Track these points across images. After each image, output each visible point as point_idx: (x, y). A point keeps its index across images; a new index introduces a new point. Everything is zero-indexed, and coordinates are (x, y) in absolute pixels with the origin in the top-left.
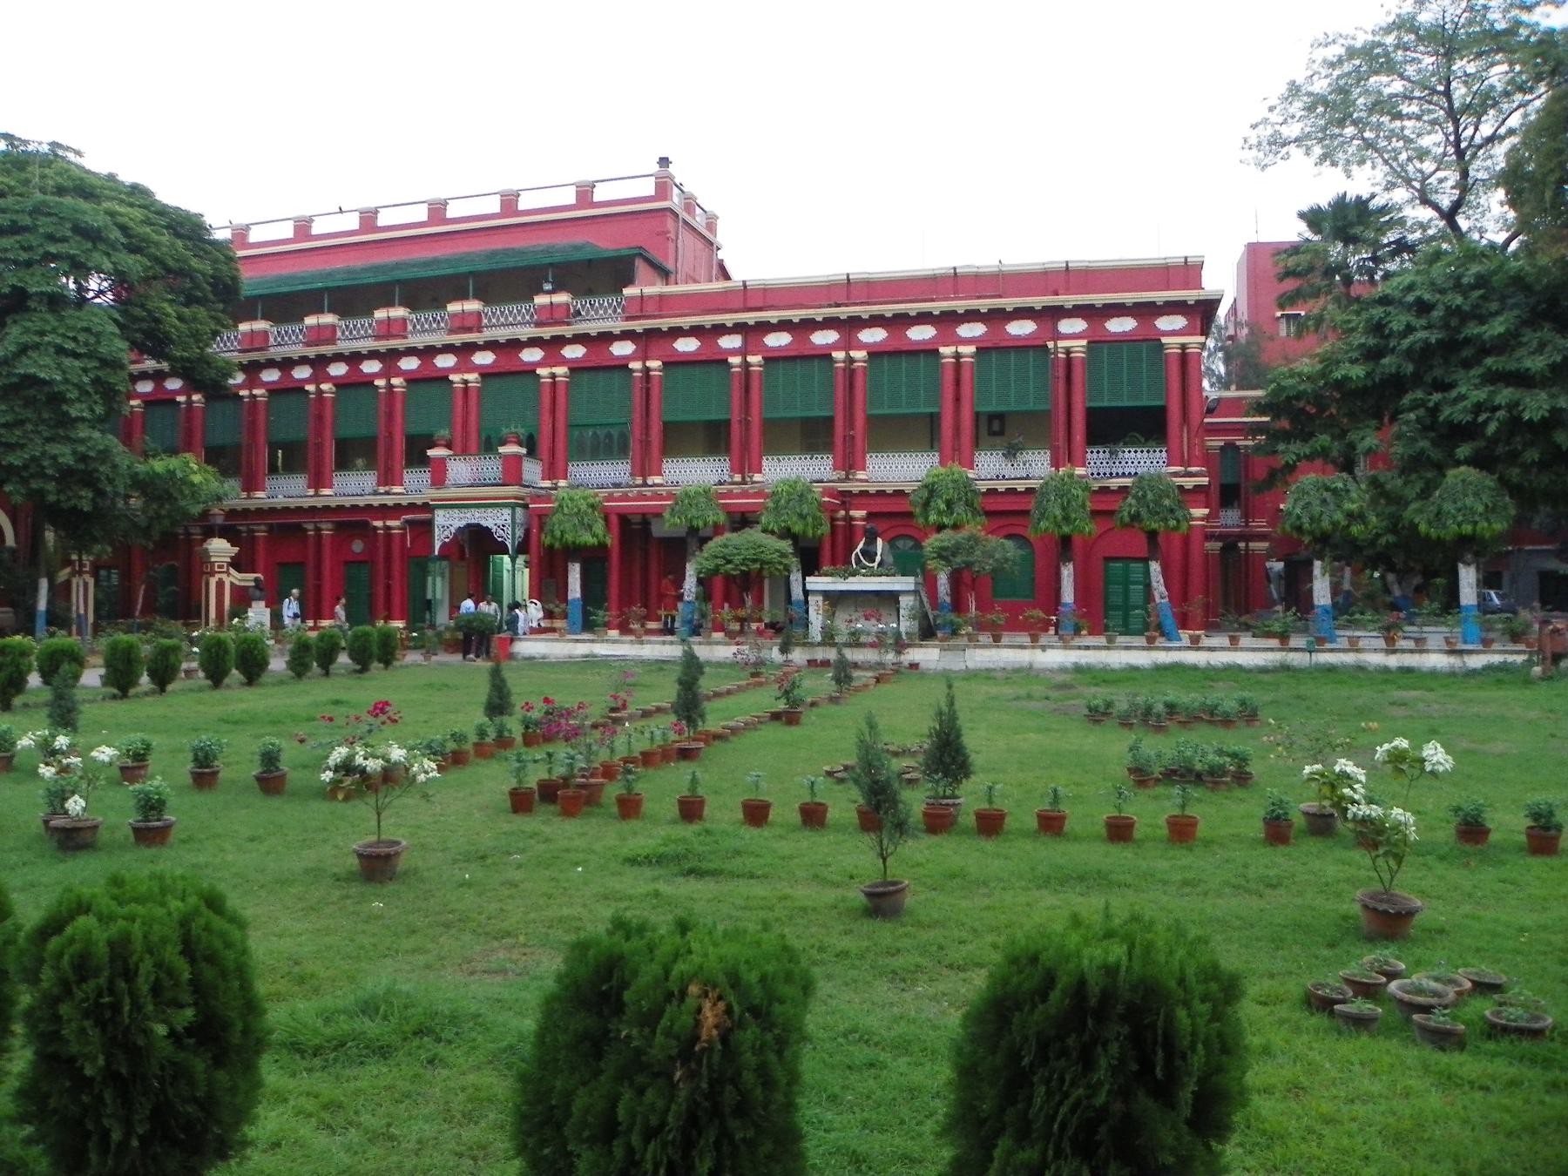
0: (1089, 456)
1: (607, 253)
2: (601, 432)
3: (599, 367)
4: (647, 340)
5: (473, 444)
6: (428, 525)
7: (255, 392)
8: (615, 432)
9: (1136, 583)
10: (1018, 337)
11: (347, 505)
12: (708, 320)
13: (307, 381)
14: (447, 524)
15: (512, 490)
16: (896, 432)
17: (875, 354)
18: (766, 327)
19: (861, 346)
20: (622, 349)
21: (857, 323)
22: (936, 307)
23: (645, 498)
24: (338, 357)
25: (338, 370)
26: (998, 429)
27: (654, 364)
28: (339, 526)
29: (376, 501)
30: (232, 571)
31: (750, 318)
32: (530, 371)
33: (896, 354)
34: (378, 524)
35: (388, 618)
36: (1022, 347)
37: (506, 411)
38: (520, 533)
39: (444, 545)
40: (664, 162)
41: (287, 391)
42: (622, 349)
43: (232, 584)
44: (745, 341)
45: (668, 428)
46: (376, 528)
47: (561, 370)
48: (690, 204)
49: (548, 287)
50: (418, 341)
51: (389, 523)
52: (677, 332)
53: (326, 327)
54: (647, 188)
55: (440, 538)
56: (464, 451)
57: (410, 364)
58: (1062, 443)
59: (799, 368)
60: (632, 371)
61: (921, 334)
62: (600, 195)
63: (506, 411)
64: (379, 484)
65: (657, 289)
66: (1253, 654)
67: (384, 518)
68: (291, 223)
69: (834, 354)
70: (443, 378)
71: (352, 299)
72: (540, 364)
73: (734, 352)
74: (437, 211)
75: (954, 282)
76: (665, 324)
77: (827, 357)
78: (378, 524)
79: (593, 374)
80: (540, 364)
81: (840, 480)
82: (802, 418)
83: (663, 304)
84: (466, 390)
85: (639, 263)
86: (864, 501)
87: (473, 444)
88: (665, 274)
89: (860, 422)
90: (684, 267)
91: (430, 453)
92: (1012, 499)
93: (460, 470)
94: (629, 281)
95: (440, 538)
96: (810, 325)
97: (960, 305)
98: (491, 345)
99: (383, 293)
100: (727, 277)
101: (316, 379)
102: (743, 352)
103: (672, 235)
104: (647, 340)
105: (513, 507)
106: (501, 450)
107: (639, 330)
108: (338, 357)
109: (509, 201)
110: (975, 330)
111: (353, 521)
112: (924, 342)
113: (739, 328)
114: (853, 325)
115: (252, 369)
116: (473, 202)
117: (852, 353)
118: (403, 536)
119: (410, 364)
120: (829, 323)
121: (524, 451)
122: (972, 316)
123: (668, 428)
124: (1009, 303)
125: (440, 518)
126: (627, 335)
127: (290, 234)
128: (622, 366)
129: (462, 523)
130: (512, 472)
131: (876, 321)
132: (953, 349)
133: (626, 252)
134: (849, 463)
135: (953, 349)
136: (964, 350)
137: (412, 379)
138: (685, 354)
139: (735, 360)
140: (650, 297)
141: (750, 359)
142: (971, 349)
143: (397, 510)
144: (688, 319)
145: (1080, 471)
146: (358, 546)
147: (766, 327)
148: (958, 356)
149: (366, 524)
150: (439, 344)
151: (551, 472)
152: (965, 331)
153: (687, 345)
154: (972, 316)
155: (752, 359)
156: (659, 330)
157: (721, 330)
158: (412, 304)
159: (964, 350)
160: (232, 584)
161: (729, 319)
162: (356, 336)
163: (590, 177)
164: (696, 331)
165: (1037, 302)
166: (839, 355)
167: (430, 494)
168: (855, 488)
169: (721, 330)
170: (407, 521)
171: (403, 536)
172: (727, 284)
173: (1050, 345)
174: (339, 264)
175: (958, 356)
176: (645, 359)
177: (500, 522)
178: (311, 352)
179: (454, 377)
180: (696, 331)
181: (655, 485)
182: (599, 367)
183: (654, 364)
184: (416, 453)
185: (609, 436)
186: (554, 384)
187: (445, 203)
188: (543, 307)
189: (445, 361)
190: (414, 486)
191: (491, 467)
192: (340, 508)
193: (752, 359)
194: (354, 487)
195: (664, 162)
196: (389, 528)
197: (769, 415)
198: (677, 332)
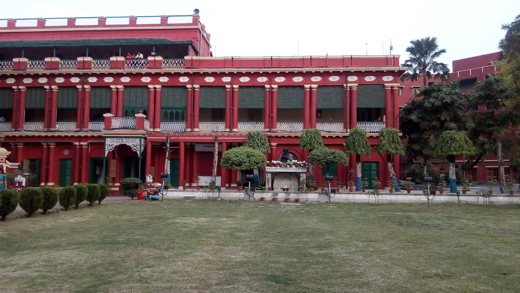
0: (358, 125)
1: (178, 43)
2: (174, 111)
3: (173, 86)
4: (194, 76)
5: (120, 113)
6: (103, 144)
7: (20, 87)
8: (180, 111)
9: (68, 176)
10: (333, 82)
11: (30, 135)
12: (218, 71)
13: (45, 84)
14: (110, 144)
15: (141, 131)
16: (289, 114)
17: (281, 86)
18: (241, 74)
19: (276, 83)
20: (184, 80)
21: (275, 75)
22: (304, 70)
23: (232, 136)
24: (60, 75)
25: (60, 80)
26: (323, 115)
27: (197, 86)
28: (58, 144)
29: (76, 135)
30: (7, 162)
31: (235, 70)
32: (145, 86)
33: (288, 87)
34: (77, 144)
35: (47, 181)
36: (334, 86)
37: (135, 101)
38: (142, 148)
39: (109, 153)
40: (197, 11)
41: (67, 87)
42: (184, 80)
43: (7, 167)
44: (232, 79)
45: (319, 111)
46: (76, 145)
47: (158, 86)
48: (203, 27)
49: (153, 53)
50: (64, 71)
51: (82, 143)
52: (206, 74)
53: (87, 62)
54: (190, 20)
55: (107, 150)
56: (116, 116)
57: (93, 80)
58: (348, 120)
59: (134, 90)
60: (188, 88)
61: (298, 80)
62: (170, 21)
63: (135, 101)
64: (12, 128)
65: (195, 58)
66: (417, 197)
67: (79, 142)
68: (36, 21)
69: (266, 86)
70: (107, 87)
71: (36, 53)
72: (150, 83)
73: (227, 83)
74: (71, 21)
75: (311, 61)
76: (202, 70)
77: (263, 87)
78: (77, 144)
79: (169, 89)
80: (150, 83)
81: (267, 132)
82: (249, 109)
83: (200, 63)
84: (351, 91)
85: (190, 47)
86: (276, 139)
87: (120, 113)
88: (197, 53)
89: (314, 111)
90: (201, 51)
91: (105, 115)
92: (290, 140)
93: (116, 123)
94: (187, 54)
95: (107, 150)
96: (293, 74)
97: (313, 70)
98: (166, 74)
99: (81, 51)
100: (211, 55)
101: (82, 83)
102: (231, 83)
103: (199, 39)
104: (194, 76)
105: (140, 138)
106: (136, 115)
107: (191, 72)
108: (60, 75)
109: (133, 20)
110: (318, 79)
111: (65, 143)
112: (336, 82)
113: (231, 74)
114: (272, 76)
115: (19, 78)
116: (87, 20)
117: (273, 86)
118: (88, 149)
119: (93, 80)
120: (265, 74)
121: (145, 116)
122: (317, 74)
123: (319, 111)
124: (331, 69)
125: (108, 142)
126: (186, 74)
127: (66, 24)
128: (183, 86)
129: (116, 144)
130: (141, 126)
131: (282, 74)
132: (309, 86)
133: (186, 43)
134: (271, 125)
135: (309, 86)
136: (313, 86)
137: (94, 86)
138: (209, 83)
139: (228, 86)
140: (196, 60)
141: (234, 86)
142: (316, 86)
143: (86, 138)
144: (219, 70)
145: (158, 130)
146: (66, 152)
147: (241, 74)
148: (311, 88)
149: (71, 144)
150: (106, 73)
151: (154, 125)
152: (314, 79)
153: (210, 80)
154: (317, 74)
155: (235, 86)
156: (199, 73)
157: (223, 74)
158: (31, 58)
159: (313, 86)
160: (7, 167)
161: (227, 70)
162: (68, 67)
163: (14, 18)
164: (213, 74)
165: (341, 69)
166: (267, 86)
167: (104, 133)
168: (274, 135)
169: (223, 74)
170: (90, 143)
171: (88, 149)
172: (210, 58)
173: (345, 85)
174: (57, 38)
175: (311, 88)
176: (192, 84)
177: (135, 144)
178: (48, 72)
179: (150, 86)
180: (213, 74)
181: (234, 132)
182: (173, 86)
183: (197, 86)
184: (97, 115)
185: (177, 112)
186: (155, 92)
187: (75, 19)
188: (80, 62)
189: (108, 80)
190: (96, 128)
191: (130, 122)
192: (27, 137)
193: (235, 86)
194: (66, 128)
195: (197, 11)
196: (82, 145)
197: (279, 107)
198: (206, 74)
